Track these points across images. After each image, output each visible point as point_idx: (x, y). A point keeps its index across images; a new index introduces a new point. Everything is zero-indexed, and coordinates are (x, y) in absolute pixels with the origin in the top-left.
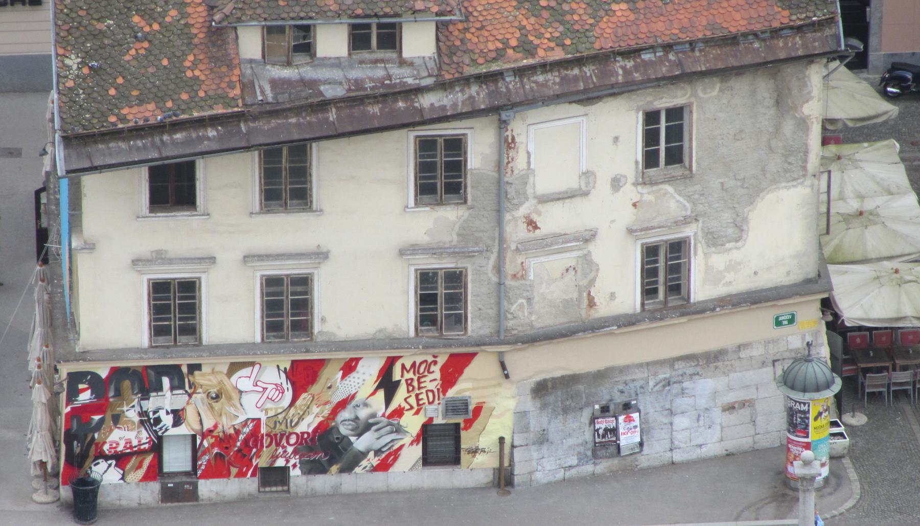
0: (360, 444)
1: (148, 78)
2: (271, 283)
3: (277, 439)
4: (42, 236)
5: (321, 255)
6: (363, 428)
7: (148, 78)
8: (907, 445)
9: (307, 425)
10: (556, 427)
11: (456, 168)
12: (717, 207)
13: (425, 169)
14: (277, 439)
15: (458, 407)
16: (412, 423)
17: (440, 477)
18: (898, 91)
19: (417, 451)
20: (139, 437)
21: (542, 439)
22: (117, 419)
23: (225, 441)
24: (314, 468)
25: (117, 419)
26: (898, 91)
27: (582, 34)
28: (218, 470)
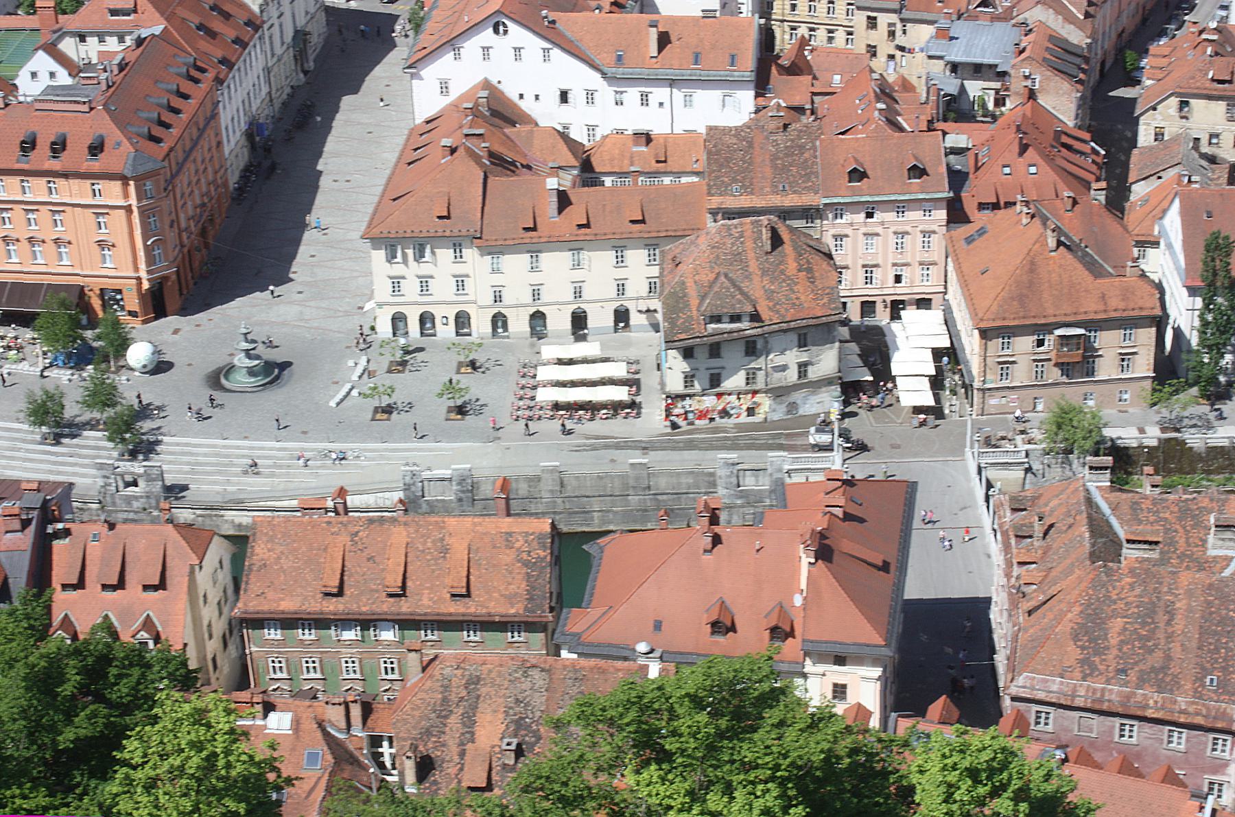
0: (732, 412)
1: (749, 679)
2: (712, 375)
3: (713, 411)
4: (658, 365)
5: (723, 368)
6: (733, 408)
7: (749, 679)
8: (164, 673)
9: (720, 408)
10: (778, 407)
11: (755, 347)
12: (469, 722)
13: (747, 348)
14: (713, 411)
15: (755, 403)
16: (745, 407)
17: (751, 419)
18: (1111, 94)
19: (746, 413)
20: (682, 411)
21: (774, 411)
22: (676, 407)
23: (701, 412)
24: (722, 417)
25: (676, 407)
26: (1111, 94)
27: (784, 316)
28: (699, 418)
